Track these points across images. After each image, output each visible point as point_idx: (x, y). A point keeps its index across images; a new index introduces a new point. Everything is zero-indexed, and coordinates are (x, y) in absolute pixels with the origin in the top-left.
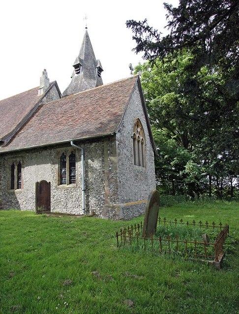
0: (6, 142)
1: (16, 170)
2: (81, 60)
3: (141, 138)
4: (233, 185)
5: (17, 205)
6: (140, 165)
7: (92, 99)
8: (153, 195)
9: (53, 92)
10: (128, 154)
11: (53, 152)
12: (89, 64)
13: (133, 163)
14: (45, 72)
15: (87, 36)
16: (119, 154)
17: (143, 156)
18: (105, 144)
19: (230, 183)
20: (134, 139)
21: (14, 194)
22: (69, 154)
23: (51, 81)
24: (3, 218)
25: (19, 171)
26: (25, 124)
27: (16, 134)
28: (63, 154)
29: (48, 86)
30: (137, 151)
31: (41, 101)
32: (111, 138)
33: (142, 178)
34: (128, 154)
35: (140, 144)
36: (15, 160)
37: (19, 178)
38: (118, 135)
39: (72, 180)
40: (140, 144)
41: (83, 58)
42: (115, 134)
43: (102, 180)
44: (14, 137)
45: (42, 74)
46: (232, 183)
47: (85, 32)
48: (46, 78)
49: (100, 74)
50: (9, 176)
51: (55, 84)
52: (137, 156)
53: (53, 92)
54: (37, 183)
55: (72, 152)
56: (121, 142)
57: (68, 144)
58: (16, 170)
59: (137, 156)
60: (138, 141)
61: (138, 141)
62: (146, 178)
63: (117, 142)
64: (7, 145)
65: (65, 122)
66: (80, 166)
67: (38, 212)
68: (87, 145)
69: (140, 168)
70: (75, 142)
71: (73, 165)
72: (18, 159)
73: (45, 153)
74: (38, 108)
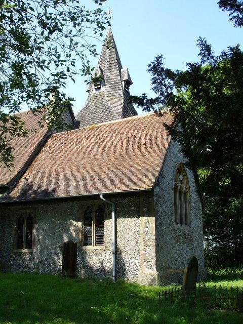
1: (25, 225)
3: (184, 187)
6: (182, 223)
7: (122, 136)
8: (191, 261)
10: (167, 210)
11: (76, 205)
13: (173, 220)
17: (186, 210)
22: (95, 208)
24: (239, 272)
28: (88, 207)
30: (178, 203)
33: (184, 239)
34: (167, 210)
35: (183, 195)
36: (23, 211)
40: (183, 195)
43: (137, 242)
49: (128, 89)
52: (178, 211)
56: (159, 197)
57: (98, 196)
58: (25, 225)
59: (178, 211)
62: (191, 239)
63: (155, 198)
65: (89, 166)
66: (109, 224)
69: (183, 227)
70: (105, 195)
71: (100, 224)
72: (28, 211)
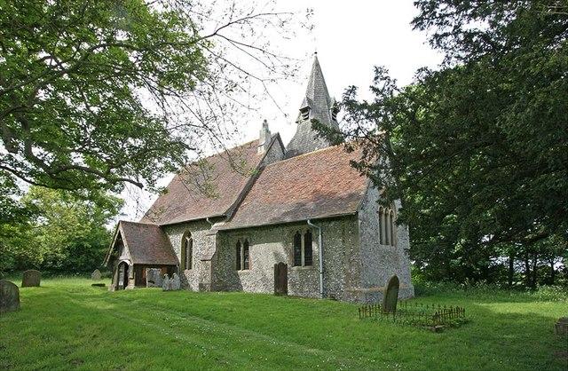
0: (229, 216)
2: (309, 101)
4: (555, 269)
5: (238, 286)
6: (387, 244)
9: (276, 148)
11: (286, 230)
12: (321, 105)
14: (265, 124)
15: (317, 65)
16: (362, 234)
18: (346, 223)
19: (550, 265)
20: (380, 213)
21: (237, 275)
23: (273, 132)
25: (246, 249)
26: (247, 192)
27: (239, 205)
29: (270, 140)
31: (262, 162)
32: (352, 218)
35: (389, 217)
37: (246, 257)
38: (361, 214)
39: (309, 261)
40: (389, 217)
41: (312, 97)
42: (357, 213)
44: (236, 210)
45: (261, 126)
46: (552, 264)
47: (314, 59)
48: (268, 131)
50: (235, 255)
51: (278, 137)
53: (276, 148)
54: (275, 265)
55: (308, 231)
57: (305, 222)
60: (386, 215)
61: (386, 215)
63: (360, 221)
64: (230, 220)
67: (277, 294)
68: (325, 224)
72: (245, 237)
73: (276, 231)
74: (261, 169)
